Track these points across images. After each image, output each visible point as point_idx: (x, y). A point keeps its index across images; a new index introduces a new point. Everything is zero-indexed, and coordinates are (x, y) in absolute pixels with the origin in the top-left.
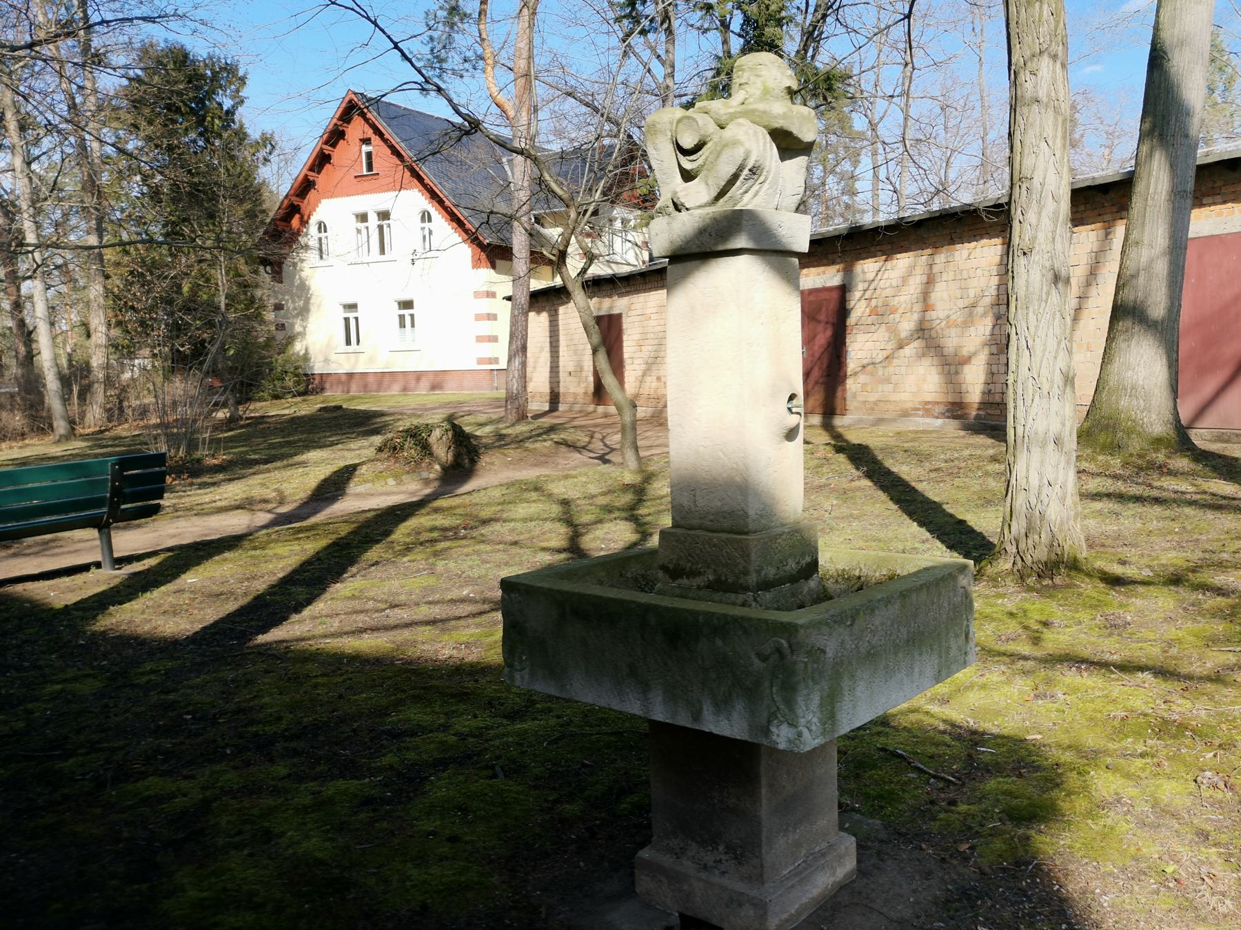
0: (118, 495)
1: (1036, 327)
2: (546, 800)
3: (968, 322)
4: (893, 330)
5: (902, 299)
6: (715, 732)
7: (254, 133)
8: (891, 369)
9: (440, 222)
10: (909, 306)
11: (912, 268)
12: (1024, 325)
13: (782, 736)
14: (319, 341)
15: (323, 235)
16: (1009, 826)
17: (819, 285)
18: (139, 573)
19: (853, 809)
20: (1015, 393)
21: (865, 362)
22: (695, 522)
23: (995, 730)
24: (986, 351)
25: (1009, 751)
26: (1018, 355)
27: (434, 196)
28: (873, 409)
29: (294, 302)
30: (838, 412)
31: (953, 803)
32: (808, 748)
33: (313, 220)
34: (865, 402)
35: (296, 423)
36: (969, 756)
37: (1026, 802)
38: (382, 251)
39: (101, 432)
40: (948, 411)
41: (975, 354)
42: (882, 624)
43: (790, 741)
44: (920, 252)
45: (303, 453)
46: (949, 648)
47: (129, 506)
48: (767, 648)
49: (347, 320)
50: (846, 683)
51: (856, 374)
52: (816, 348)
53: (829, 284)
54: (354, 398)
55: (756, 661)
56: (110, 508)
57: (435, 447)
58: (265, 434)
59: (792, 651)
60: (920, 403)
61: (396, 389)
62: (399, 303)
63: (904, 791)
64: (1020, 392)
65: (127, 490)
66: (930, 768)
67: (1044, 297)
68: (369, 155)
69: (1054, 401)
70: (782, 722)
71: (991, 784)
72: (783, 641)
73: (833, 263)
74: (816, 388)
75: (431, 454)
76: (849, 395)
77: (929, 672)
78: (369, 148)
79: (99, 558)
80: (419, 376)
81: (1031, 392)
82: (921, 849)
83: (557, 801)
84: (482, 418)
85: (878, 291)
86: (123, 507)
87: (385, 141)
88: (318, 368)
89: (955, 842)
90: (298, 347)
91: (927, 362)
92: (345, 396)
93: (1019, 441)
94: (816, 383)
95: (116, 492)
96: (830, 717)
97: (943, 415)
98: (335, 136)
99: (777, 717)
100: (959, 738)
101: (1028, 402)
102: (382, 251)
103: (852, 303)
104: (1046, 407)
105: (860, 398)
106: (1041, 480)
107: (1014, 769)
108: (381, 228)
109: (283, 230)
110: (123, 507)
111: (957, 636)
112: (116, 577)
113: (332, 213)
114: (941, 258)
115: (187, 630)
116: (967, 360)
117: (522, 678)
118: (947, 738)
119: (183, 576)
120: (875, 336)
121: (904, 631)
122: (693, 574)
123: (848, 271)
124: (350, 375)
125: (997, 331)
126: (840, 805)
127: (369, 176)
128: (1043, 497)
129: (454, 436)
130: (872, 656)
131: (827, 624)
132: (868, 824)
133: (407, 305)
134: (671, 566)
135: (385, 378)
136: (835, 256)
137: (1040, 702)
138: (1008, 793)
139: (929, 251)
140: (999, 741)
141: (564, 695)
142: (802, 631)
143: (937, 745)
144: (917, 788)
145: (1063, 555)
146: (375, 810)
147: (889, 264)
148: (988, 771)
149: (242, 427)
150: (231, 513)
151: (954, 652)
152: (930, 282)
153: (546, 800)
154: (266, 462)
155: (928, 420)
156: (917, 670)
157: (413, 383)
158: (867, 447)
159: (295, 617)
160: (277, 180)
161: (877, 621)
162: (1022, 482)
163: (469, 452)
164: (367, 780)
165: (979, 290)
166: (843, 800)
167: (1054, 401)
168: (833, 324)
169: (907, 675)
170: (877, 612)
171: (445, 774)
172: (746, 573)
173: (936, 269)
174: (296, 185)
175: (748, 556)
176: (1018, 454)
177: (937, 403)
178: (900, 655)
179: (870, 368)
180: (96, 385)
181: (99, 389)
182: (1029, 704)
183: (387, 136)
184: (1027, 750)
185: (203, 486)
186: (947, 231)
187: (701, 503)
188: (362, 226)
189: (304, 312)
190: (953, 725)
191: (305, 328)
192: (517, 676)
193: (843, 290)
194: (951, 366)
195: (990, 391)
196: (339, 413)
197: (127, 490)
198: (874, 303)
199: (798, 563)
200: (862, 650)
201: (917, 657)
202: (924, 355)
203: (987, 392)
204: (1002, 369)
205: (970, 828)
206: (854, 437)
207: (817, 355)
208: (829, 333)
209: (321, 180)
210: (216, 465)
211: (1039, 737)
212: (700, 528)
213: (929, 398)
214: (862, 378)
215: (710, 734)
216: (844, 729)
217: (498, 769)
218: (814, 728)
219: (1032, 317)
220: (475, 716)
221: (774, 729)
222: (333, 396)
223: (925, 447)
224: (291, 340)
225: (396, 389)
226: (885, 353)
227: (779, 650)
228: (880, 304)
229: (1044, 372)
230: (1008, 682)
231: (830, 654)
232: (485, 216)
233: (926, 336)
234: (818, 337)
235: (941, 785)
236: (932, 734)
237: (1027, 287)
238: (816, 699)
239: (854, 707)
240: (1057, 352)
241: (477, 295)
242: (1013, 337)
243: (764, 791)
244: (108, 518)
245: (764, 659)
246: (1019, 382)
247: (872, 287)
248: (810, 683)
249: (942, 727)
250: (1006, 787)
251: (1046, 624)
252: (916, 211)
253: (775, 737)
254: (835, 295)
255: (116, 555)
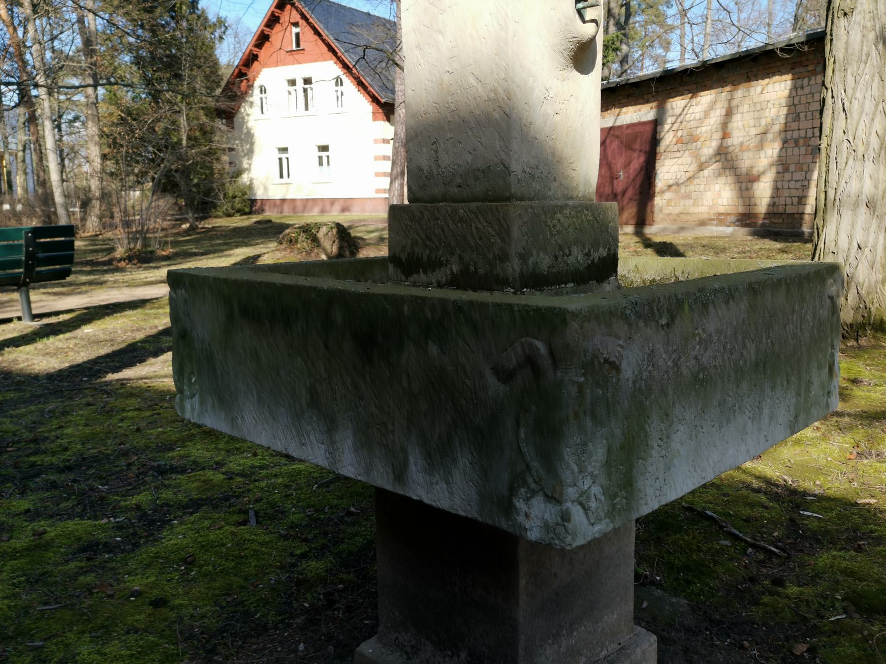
0: (32, 260)
1: (854, 89)
2: (292, 554)
3: (760, 146)
4: (697, 156)
5: (704, 129)
6: (426, 500)
7: (212, 18)
8: (692, 188)
9: (349, 85)
10: (709, 136)
11: (712, 106)
12: (841, 87)
13: (534, 517)
14: (261, 176)
15: (263, 95)
16: (857, 620)
17: (635, 121)
18: (51, 324)
19: (653, 583)
20: (828, 156)
21: (671, 182)
22: (437, 191)
23: (818, 491)
24: (774, 170)
25: (839, 517)
26: (833, 118)
27: (345, 66)
28: (675, 220)
29: (242, 146)
30: (647, 222)
31: (778, 582)
32: (580, 541)
33: (257, 84)
34: (669, 214)
35: (237, 231)
36: (792, 520)
37: (875, 587)
38: (307, 109)
39: (97, 235)
40: (738, 220)
41: (764, 173)
42: (719, 332)
43: (546, 526)
44: (720, 89)
45: (232, 249)
46: (810, 382)
47: (44, 269)
48: (511, 358)
49: (280, 159)
50: (655, 427)
51: (663, 192)
52: (631, 171)
53: (644, 119)
54: (285, 217)
55: (492, 381)
56: (25, 269)
57: (322, 240)
58: (211, 238)
59: (555, 363)
60: (714, 214)
61: (316, 211)
62: (319, 147)
63: (716, 563)
64: (833, 155)
65: (41, 255)
66: (745, 533)
67: (864, 58)
68: (297, 35)
69: (869, 165)
70: (534, 493)
71: (824, 558)
72: (539, 344)
73: (648, 102)
74: (630, 204)
75: (319, 246)
76: (656, 209)
77: (784, 416)
78: (297, 30)
79: (19, 314)
80: (333, 201)
81: (845, 154)
82: (742, 647)
83: (304, 556)
84: (371, 228)
85: (684, 124)
86: (38, 269)
87: (309, 24)
88: (260, 194)
89: (787, 639)
90: (245, 178)
91: (722, 180)
92: (279, 215)
93: (829, 204)
94: (630, 199)
95: (29, 256)
96: (623, 481)
97: (733, 224)
98: (272, 21)
99: (525, 483)
100: (776, 497)
101: (842, 164)
102: (307, 109)
103: (663, 134)
104: (860, 169)
105: (666, 211)
106: (850, 244)
107: (848, 540)
108: (305, 90)
109: (234, 90)
110: (38, 269)
111: (820, 367)
112: (31, 327)
113: (270, 77)
114: (739, 93)
115: (54, 368)
116: (756, 179)
117: (193, 409)
118: (763, 498)
119: (83, 327)
120: (680, 161)
121: (751, 347)
122: (433, 265)
123: (661, 110)
124: (283, 201)
125: (783, 153)
126: (637, 577)
127: (298, 52)
128: (852, 260)
129: (338, 232)
130: (700, 383)
131: (626, 318)
132: (672, 604)
133: (324, 148)
134: (404, 257)
135: (308, 203)
136: (650, 96)
137: (865, 461)
138: (848, 573)
139: (728, 88)
140: (825, 504)
141: (235, 434)
142: (575, 325)
143: (752, 505)
144: (731, 559)
145: (869, 317)
146: (89, 559)
147: (694, 101)
148: (818, 541)
149: (198, 233)
150: (155, 286)
151: (815, 389)
152: (729, 113)
153: (292, 554)
154: (202, 254)
155: (721, 228)
156: (766, 411)
157: (328, 207)
158: (671, 244)
159: (152, 360)
160: (228, 54)
161: (712, 324)
162: (831, 246)
163: (350, 246)
164: (105, 521)
165: (769, 120)
166: (641, 571)
167: (869, 165)
168: (646, 152)
169: (753, 419)
170: (711, 309)
171: (192, 518)
172: (504, 257)
173: (734, 103)
174: (245, 57)
175: (508, 231)
176: (828, 217)
177: (729, 214)
178: (745, 386)
179: (674, 188)
180: (94, 202)
181: (96, 203)
182: (852, 463)
183: (311, 20)
184: (861, 516)
185: (146, 269)
186: (745, 71)
187: (446, 160)
188: (292, 89)
189: (250, 153)
190: (768, 481)
191: (250, 165)
192: (188, 406)
193: (656, 124)
194: (745, 182)
195: (774, 204)
196: (269, 225)
197: (41, 255)
198: (680, 133)
199: (588, 255)
200: (685, 371)
201: (768, 391)
202: (720, 175)
203: (773, 205)
204: (817, 131)
205: (805, 620)
206: (657, 239)
207: (632, 177)
208: (642, 159)
209: (263, 54)
210: (163, 256)
211: (873, 501)
212: (444, 199)
213: (722, 210)
214: (668, 195)
215: (420, 503)
216: (649, 504)
217: (251, 514)
218: (593, 504)
219: (850, 79)
220: (255, 455)
221: (520, 504)
222: (270, 214)
223: (720, 243)
224: (239, 173)
225: (316, 211)
226: (688, 175)
227: (531, 361)
228: (685, 134)
229: (861, 133)
230: (825, 438)
231: (628, 371)
232: (360, 51)
233: (725, 158)
234: (633, 163)
235: (761, 557)
236: (744, 492)
237: (846, 49)
238: (598, 454)
239: (668, 468)
240: (874, 114)
241: (376, 141)
242: (829, 101)
243: (522, 583)
244: (25, 278)
245: (505, 376)
246: (833, 145)
247: (679, 120)
248: (589, 423)
249: (756, 484)
250: (844, 564)
251: (855, 381)
252: (720, 52)
253: (521, 519)
254: (649, 128)
255: (34, 312)
